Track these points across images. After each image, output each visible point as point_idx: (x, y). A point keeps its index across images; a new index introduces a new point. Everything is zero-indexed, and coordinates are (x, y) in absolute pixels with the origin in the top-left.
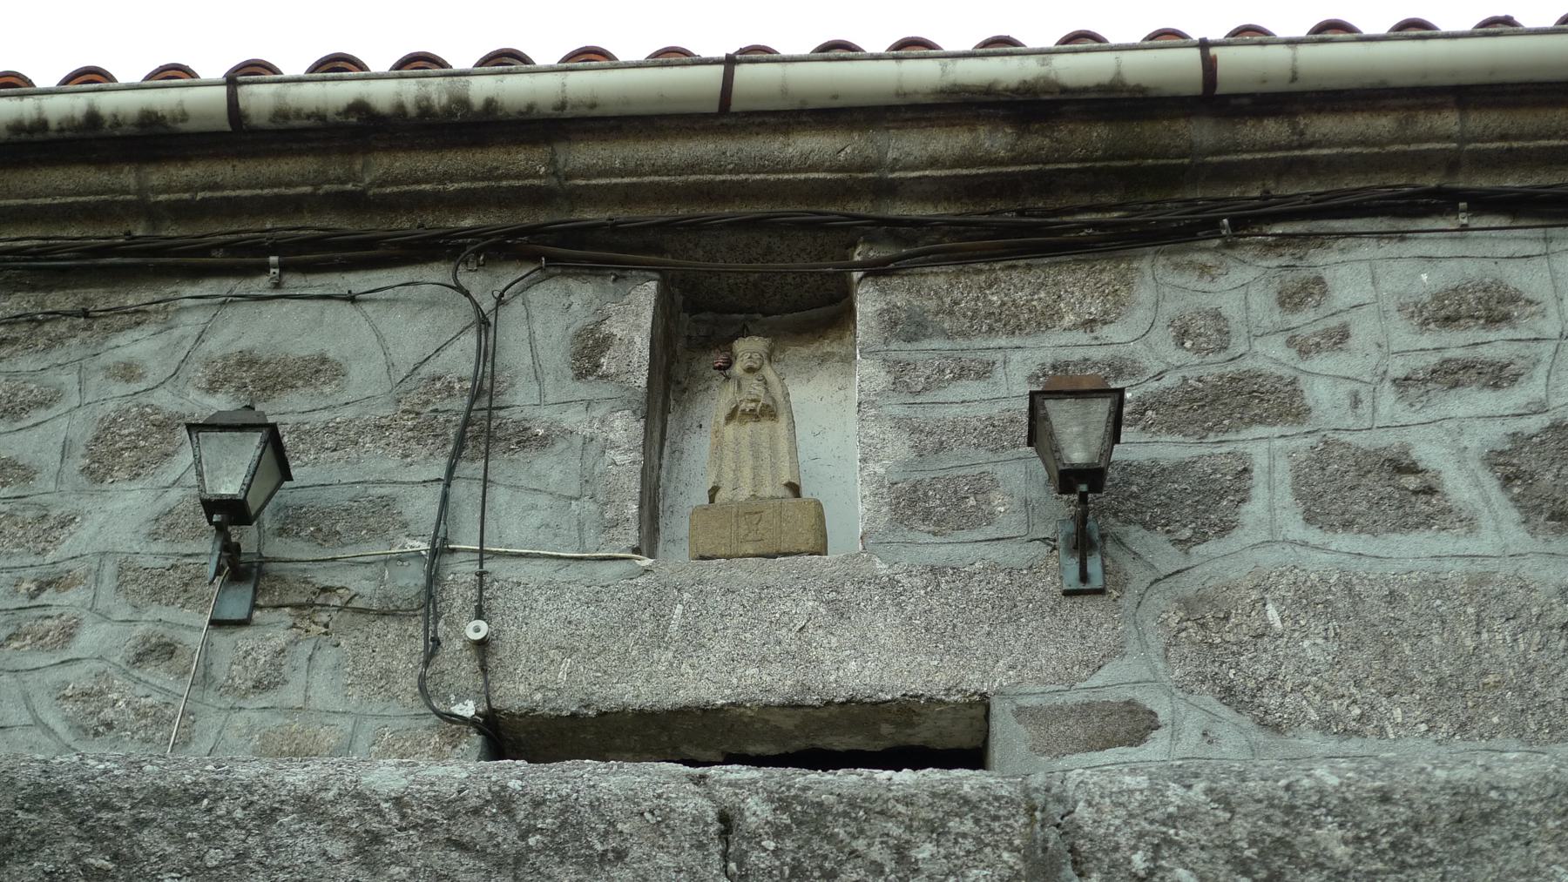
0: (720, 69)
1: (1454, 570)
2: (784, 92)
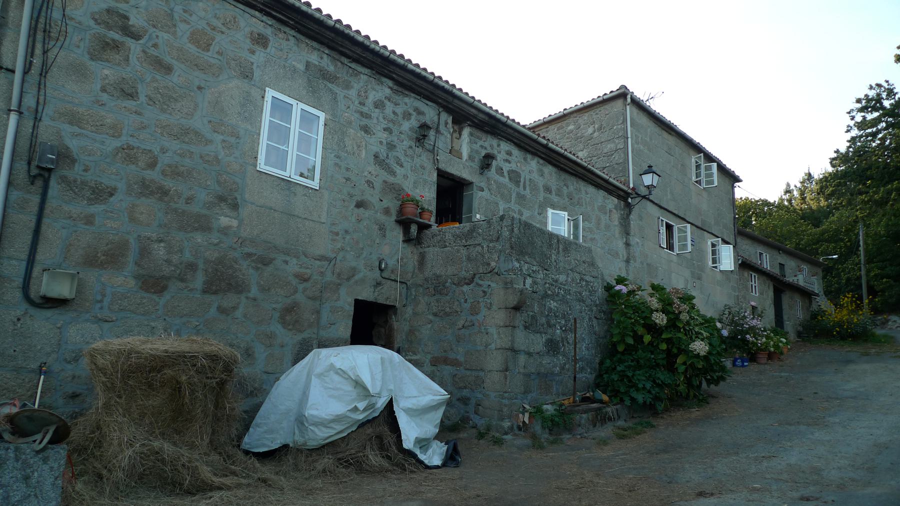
0: (786, 299)
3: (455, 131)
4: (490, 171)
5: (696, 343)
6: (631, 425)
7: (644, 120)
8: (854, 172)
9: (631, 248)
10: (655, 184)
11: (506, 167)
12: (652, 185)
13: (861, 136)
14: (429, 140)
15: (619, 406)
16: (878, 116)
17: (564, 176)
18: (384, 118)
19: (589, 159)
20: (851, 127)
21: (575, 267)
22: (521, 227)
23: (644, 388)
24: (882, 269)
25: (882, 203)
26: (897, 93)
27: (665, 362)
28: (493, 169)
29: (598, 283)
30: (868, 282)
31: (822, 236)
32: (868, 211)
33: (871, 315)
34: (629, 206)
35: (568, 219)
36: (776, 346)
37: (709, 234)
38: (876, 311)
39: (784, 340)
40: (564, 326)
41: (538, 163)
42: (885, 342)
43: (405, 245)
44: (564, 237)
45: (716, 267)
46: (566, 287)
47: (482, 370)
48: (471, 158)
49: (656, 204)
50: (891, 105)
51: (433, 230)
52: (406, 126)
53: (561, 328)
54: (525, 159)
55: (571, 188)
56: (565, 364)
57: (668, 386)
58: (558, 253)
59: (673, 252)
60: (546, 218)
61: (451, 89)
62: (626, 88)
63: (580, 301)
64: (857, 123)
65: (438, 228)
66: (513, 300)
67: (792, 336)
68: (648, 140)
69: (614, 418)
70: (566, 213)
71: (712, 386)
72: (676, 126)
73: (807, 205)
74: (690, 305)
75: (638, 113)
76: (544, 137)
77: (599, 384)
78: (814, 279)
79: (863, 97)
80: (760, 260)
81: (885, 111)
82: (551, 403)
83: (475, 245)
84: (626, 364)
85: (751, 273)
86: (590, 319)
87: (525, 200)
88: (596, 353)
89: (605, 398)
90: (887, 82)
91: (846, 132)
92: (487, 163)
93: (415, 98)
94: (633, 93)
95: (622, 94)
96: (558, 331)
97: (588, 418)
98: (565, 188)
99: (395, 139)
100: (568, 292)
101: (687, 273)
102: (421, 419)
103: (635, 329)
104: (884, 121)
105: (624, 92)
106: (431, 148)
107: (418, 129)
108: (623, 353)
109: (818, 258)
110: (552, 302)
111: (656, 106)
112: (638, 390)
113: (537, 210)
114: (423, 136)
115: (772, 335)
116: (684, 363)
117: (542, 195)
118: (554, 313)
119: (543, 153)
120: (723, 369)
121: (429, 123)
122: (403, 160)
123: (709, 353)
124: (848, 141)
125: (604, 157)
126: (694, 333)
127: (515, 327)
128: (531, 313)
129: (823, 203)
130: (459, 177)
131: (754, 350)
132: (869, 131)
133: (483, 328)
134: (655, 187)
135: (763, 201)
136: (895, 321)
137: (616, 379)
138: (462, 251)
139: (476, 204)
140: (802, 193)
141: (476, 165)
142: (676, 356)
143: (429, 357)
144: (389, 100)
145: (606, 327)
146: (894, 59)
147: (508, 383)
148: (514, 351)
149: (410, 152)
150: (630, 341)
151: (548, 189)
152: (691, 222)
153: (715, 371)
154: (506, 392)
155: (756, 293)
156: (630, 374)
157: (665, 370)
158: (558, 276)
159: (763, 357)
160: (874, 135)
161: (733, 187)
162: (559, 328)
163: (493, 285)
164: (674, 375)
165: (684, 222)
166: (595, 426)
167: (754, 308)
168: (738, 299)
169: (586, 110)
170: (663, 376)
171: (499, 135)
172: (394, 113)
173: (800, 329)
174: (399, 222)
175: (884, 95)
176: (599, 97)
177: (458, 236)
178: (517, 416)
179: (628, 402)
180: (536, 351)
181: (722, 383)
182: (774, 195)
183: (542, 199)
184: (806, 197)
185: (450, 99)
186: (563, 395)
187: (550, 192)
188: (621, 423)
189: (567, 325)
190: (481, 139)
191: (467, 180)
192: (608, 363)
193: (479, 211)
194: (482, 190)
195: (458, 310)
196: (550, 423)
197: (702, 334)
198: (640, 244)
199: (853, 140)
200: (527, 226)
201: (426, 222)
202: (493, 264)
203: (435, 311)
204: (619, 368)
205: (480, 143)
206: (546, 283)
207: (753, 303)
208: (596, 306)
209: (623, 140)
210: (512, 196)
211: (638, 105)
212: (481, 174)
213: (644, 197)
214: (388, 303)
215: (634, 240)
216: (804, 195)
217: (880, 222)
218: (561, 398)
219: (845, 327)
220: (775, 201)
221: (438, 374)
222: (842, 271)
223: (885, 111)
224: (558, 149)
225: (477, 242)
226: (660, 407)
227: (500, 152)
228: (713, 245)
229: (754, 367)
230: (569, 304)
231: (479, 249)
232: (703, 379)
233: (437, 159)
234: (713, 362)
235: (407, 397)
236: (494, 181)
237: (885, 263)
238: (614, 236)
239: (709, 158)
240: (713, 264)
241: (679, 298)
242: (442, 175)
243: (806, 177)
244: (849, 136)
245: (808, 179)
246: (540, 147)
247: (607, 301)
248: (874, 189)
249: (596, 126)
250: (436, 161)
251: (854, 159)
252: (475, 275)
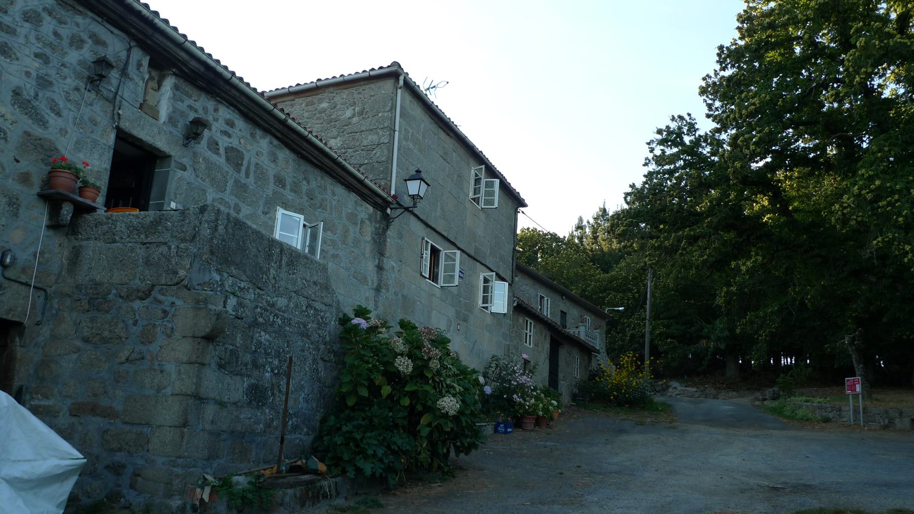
0: (563, 353)
1: (217, 163)
2: (237, 85)
3: (151, 78)
4: (199, 143)
5: (445, 399)
6: (352, 504)
7: (417, 111)
8: (647, 212)
9: (385, 273)
10: (422, 194)
11: (224, 142)
12: (418, 195)
13: (658, 173)
14: (109, 83)
15: (340, 478)
16: (677, 152)
17: (305, 166)
18: (38, 39)
19: (343, 150)
20: (650, 161)
21: (302, 288)
22: (230, 225)
23: (375, 455)
24: (667, 327)
25: (671, 251)
26: (698, 129)
27: (405, 423)
28: (204, 142)
29: (331, 313)
30: (651, 341)
31: (610, 283)
32: (657, 259)
33: (651, 378)
34: (387, 220)
35: (304, 226)
36: (546, 410)
37: (482, 266)
38: (657, 375)
39: (555, 403)
40: (277, 367)
41: (271, 143)
42: (662, 411)
43: (51, 233)
44: (296, 248)
45: (486, 308)
46: (286, 315)
47: (148, 424)
48: (171, 120)
49: (422, 221)
50: (691, 141)
51: (98, 215)
52: (73, 56)
53: (272, 371)
54: (253, 135)
55: (314, 184)
56: (272, 420)
57: (406, 453)
58: (280, 267)
59: (437, 284)
60: (273, 219)
61: (151, 16)
62: (400, 66)
63: (303, 336)
64: (656, 156)
65: (106, 214)
66: (205, 326)
67: (566, 399)
68: (421, 138)
69: (331, 496)
70: (302, 217)
71: (462, 455)
72: (456, 126)
73: (599, 246)
74: (443, 350)
75: (411, 101)
76: (282, 110)
77: (317, 449)
78: (597, 333)
79: (664, 128)
80: (541, 305)
81: (684, 148)
82: (245, 474)
83: (159, 244)
84: (355, 423)
85: (527, 318)
86: (314, 360)
87: (245, 192)
88: (317, 407)
89: (322, 467)
90: (689, 115)
91: (644, 165)
92: (194, 131)
93: (94, 19)
94: (407, 74)
95: (394, 74)
96: (267, 374)
97: (295, 496)
98: (305, 183)
99: (53, 72)
100: (288, 321)
101: (451, 312)
102: (35, 494)
103: (372, 377)
104: (682, 159)
105: (397, 70)
106: (111, 96)
107: (92, 65)
108: (353, 409)
109: (604, 310)
110: (263, 333)
111: (437, 99)
112: (366, 457)
113: (261, 208)
114: (99, 75)
115: (543, 395)
116: (429, 425)
117: (271, 187)
118: (264, 348)
119: (278, 131)
120: (476, 434)
121: (111, 59)
122: (61, 106)
123: (461, 412)
124: (645, 176)
125: (362, 150)
126: (445, 386)
127: (203, 365)
128: (231, 347)
129: (615, 245)
130: (150, 146)
131: (520, 414)
132: (667, 167)
133: (157, 363)
134: (422, 198)
135: (551, 234)
136: (675, 388)
137: (339, 443)
138: (138, 251)
139: (172, 186)
140: (595, 231)
141: (178, 132)
142: (421, 414)
143: (69, 402)
144: (50, 14)
145: (335, 373)
146: (698, 91)
147: (184, 444)
148: (199, 398)
149: (75, 96)
150: (364, 393)
151: (280, 181)
152: (462, 248)
153: (467, 437)
154: (180, 457)
155: (530, 344)
156: (358, 437)
157: (404, 432)
158: (275, 299)
159: (529, 423)
160: (671, 173)
161: (516, 212)
162: (269, 370)
163: (179, 303)
164: (416, 440)
165: (453, 247)
166: (303, 506)
167: (526, 362)
168: (509, 350)
169: (347, 86)
170: (400, 440)
171: (218, 95)
172: (56, 34)
173: (576, 391)
174: (42, 197)
175: (685, 130)
176: (364, 71)
177: (135, 228)
178: (193, 490)
179: (351, 474)
180: (232, 400)
181: (473, 452)
182: (564, 230)
183: (270, 193)
184: (598, 236)
185: (150, 31)
186: (265, 463)
187: (284, 186)
188: (340, 502)
189: (281, 367)
190: (190, 97)
191: (161, 151)
192: (332, 420)
193: (176, 198)
194: (184, 168)
195: (122, 335)
196: (239, 501)
197: (454, 388)
198: (396, 269)
199: (650, 175)
200: (239, 224)
201: (89, 202)
202: (182, 273)
203: (85, 334)
204: (344, 429)
205: (188, 102)
206: (257, 307)
207: (525, 356)
208: (325, 344)
209: (388, 133)
210: (228, 184)
211: (411, 88)
212: (185, 145)
213: (407, 209)
214: (10, 317)
215: (389, 263)
216: (596, 233)
217: (669, 274)
218: (262, 466)
219: (623, 391)
220: (565, 237)
221: (80, 428)
222: (628, 326)
223: (684, 148)
224: (299, 128)
225: (161, 240)
226: (393, 480)
227: (216, 120)
228: (486, 281)
229: (518, 434)
230: (288, 338)
231: (164, 249)
232: (451, 445)
233: (119, 114)
234: (464, 424)
235: (14, 461)
236: (204, 159)
237: (671, 321)
238: (364, 255)
239: (492, 172)
240: (483, 303)
241: (431, 340)
242: (123, 137)
243: (601, 213)
244: (646, 170)
245: (603, 216)
246: (276, 122)
247: (341, 338)
248: (666, 234)
249: (357, 109)
250: (116, 117)
251: (648, 197)
252: (153, 286)
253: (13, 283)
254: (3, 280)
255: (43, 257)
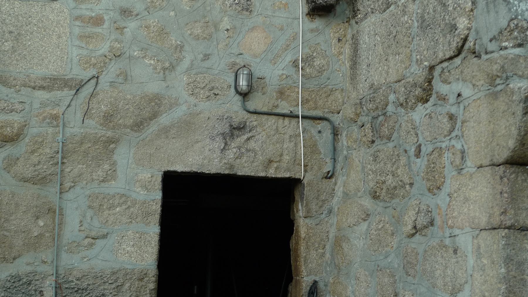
43: (318, 23)
214: (272, 173)
253: (266, 117)
254: (247, 115)
255: (311, 66)
